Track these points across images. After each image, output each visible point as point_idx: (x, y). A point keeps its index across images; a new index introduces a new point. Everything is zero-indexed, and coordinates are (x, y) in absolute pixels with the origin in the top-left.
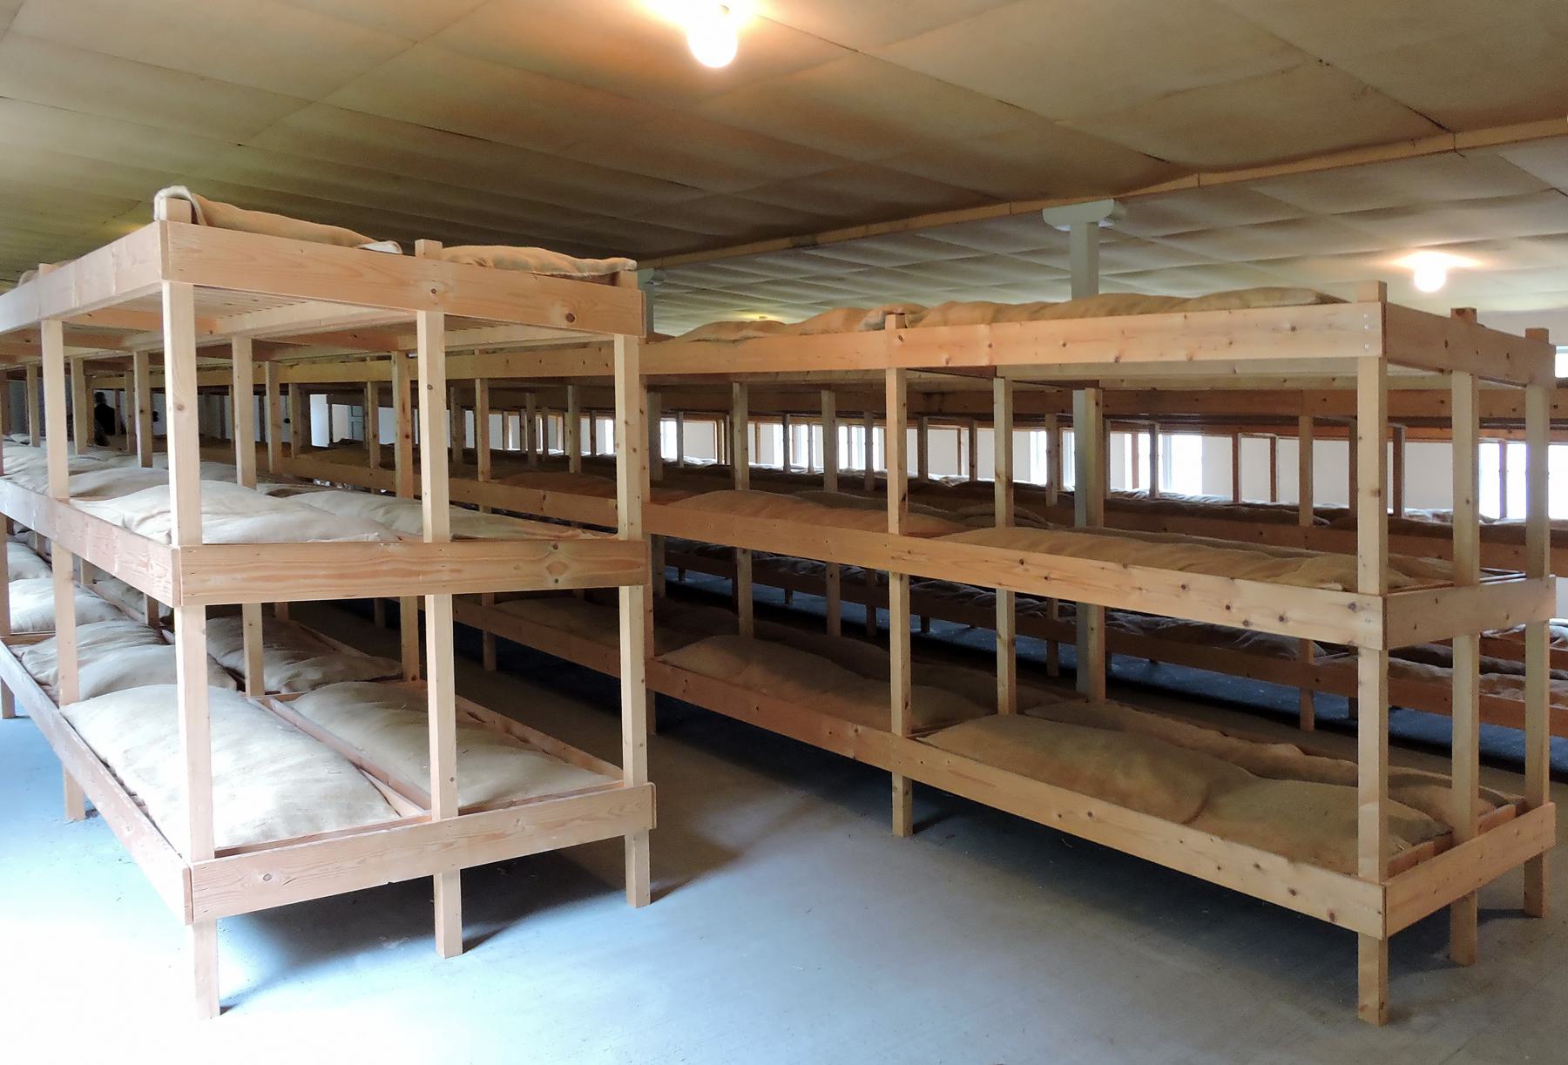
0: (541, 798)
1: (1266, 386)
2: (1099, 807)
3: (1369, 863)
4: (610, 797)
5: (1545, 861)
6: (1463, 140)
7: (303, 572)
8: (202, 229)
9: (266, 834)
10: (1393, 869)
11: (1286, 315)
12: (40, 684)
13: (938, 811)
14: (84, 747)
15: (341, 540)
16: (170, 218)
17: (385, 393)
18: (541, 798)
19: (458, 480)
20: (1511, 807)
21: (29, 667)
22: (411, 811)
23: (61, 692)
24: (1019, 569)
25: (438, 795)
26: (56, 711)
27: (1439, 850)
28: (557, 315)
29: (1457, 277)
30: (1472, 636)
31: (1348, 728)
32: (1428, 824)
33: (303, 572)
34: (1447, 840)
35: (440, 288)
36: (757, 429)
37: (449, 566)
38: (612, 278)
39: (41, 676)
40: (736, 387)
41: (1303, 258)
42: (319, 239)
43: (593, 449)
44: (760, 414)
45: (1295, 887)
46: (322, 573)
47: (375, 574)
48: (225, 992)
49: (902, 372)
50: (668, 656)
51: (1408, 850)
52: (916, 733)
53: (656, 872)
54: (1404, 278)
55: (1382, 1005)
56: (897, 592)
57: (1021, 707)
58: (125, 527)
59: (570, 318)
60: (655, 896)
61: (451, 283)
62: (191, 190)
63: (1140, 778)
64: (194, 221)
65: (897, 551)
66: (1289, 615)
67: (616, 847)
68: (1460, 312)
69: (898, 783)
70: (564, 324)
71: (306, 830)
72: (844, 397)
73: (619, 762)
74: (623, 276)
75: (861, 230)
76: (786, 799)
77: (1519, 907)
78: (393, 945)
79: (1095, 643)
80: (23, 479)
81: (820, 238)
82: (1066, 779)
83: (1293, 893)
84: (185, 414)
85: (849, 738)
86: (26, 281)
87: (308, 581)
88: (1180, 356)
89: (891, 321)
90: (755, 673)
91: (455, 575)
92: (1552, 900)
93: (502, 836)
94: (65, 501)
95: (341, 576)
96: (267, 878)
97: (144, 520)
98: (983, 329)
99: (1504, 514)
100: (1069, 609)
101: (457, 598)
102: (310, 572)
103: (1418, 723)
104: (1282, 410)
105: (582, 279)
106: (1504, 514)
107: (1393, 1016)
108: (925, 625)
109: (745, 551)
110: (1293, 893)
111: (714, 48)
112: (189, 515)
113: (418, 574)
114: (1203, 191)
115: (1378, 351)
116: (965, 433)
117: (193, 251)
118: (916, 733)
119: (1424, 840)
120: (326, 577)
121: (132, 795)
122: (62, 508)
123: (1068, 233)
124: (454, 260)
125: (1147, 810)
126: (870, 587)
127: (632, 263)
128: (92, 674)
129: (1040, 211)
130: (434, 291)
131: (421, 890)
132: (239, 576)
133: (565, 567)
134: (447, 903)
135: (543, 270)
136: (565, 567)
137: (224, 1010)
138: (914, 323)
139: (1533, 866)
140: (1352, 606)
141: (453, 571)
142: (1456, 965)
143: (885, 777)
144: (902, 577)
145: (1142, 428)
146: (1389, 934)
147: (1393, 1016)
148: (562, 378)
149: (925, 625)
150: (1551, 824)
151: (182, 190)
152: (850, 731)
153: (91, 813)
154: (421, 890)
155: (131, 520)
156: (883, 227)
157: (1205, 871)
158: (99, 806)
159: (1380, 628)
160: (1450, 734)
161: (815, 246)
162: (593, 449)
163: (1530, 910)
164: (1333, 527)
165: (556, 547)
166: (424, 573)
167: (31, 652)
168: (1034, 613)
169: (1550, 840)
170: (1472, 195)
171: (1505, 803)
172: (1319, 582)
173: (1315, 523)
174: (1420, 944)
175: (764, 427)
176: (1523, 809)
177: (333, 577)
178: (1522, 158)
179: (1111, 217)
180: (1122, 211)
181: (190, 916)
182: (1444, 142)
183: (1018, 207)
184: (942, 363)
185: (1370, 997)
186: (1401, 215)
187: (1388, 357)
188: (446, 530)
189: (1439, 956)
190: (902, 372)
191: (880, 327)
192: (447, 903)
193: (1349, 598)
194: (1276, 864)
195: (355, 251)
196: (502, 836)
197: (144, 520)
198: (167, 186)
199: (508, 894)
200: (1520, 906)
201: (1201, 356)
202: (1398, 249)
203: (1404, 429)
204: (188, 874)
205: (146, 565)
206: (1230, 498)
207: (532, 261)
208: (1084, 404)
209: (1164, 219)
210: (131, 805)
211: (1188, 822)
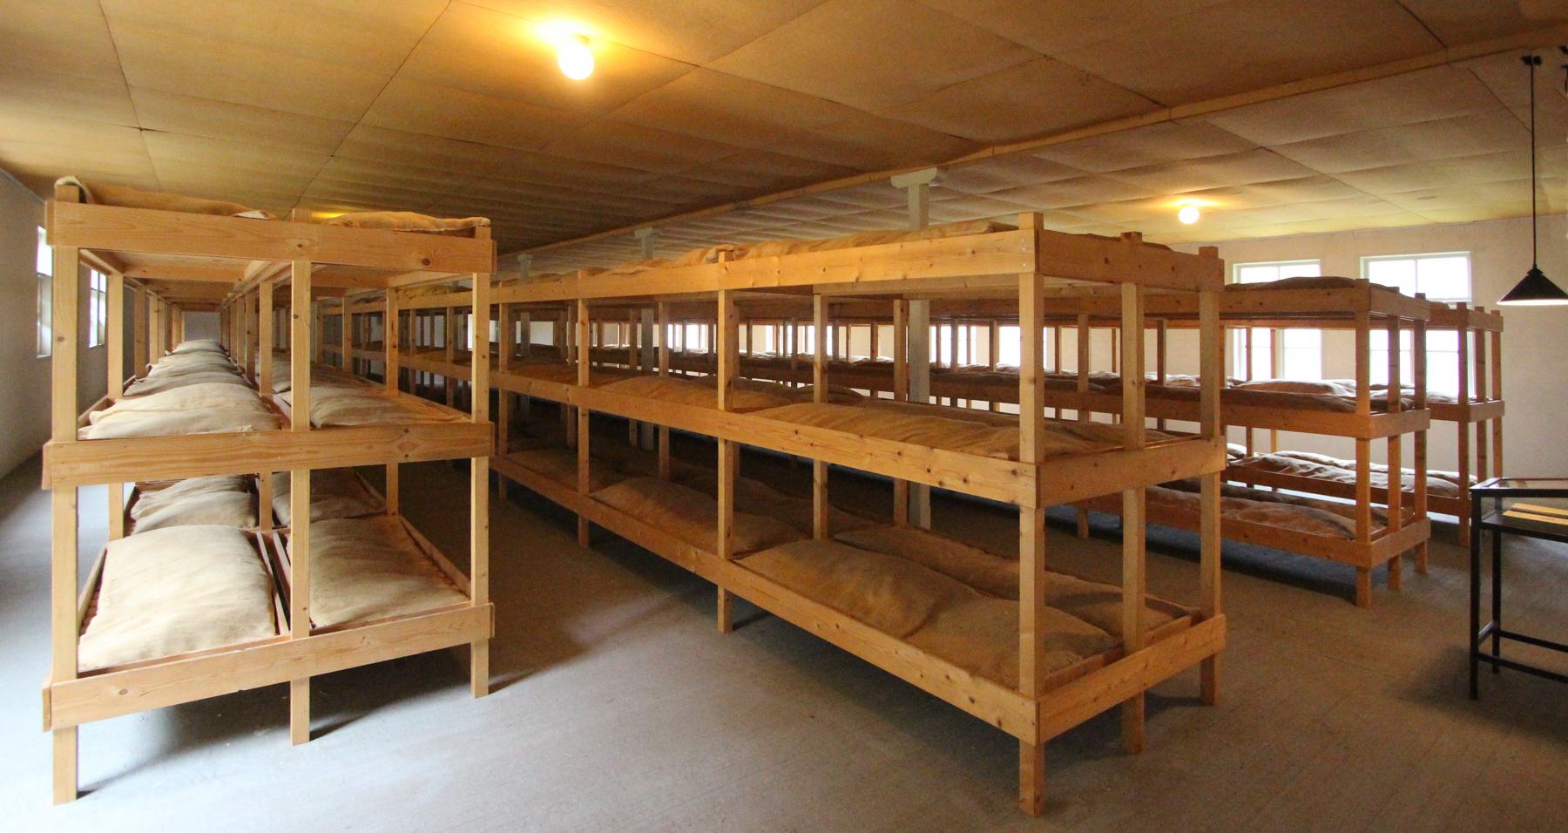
0: (394, 619)
1: (998, 296)
2: (844, 621)
3: (1027, 681)
4: (460, 615)
5: (1217, 662)
6: (1177, 112)
8: (91, 208)
9: (143, 655)
10: (1048, 686)
11: (969, 241)
18: (394, 619)
20: (1187, 619)
24: (795, 438)
25: (347, 620)
27: (1109, 661)
29: (1208, 215)
30: (1138, 490)
31: (1115, 537)
32: (1102, 639)
34: (1118, 652)
35: (306, 243)
36: (749, 329)
40: (817, 301)
41: (1094, 205)
43: (600, 342)
44: (675, 319)
45: (975, 697)
48: (82, 785)
49: (728, 293)
50: (598, 494)
51: (1079, 662)
52: (736, 556)
53: (493, 670)
54: (1171, 217)
55: (1037, 800)
57: (831, 531)
59: (426, 262)
60: (493, 689)
63: (882, 600)
66: (970, 478)
67: (465, 649)
68: (1127, 235)
69: (721, 593)
72: (711, 308)
74: (478, 231)
75: (775, 196)
76: (659, 597)
77: (1186, 700)
78: (260, 734)
81: (751, 203)
82: (826, 599)
83: (972, 701)
85: (692, 559)
88: (898, 276)
89: (722, 255)
90: (648, 507)
92: (1225, 689)
93: (349, 650)
95: (204, 460)
96: (123, 692)
98: (775, 259)
99: (1249, 377)
103: (1168, 533)
104: (1068, 311)
105: (440, 233)
106: (1249, 377)
107: (1048, 807)
110: (972, 701)
113: (276, 455)
114: (996, 159)
115: (1032, 268)
118: (736, 556)
119: (1097, 652)
125: (879, 626)
127: (486, 220)
131: (283, 689)
132: (106, 463)
133: (415, 446)
134: (300, 702)
135: (402, 228)
136: (415, 446)
137: (80, 794)
138: (740, 257)
139: (1208, 664)
140: (1014, 472)
142: (1126, 753)
143: (713, 588)
145: (961, 323)
146: (1044, 739)
147: (1048, 807)
148: (562, 302)
150: (1221, 630)
154: (283, 689)
156: (791, 193)
157: (912, 678)
159: (1033, 490)
160: (1147, 560)
161: (749, 208)
162: (600, 342)
163: (1205, 699)
164: (1104, 392)
169: (1220, 644)
170: (1211, 154)
171: (1185, 614)
172: (991, 452)
173: (1091, 389)
174: (1091, 741)
175: (756, 329)
176: (1198, 619)
178: (1222, 122)
179: (936, 180)
180: (943, 176)
181: (48, 724)
182: (1163, 115)
183: (876, 176)
184: (775, 284)
185: (1027, 794)
186: (1159, 171)
187: (1040, 271)
189: (1113, 744)
190: (728, 293)
191: (715, 260)
192: (300, 702)
193: (1013, 465)
194: (961, 676)
195: (228, 220)
196: (349, 650)
199: (348, 695)
200: (1197, 695)
201: (913, 275)
203: (1166, 322)
204: (48, 694)
209: (986, 181)
211: (905, 638)
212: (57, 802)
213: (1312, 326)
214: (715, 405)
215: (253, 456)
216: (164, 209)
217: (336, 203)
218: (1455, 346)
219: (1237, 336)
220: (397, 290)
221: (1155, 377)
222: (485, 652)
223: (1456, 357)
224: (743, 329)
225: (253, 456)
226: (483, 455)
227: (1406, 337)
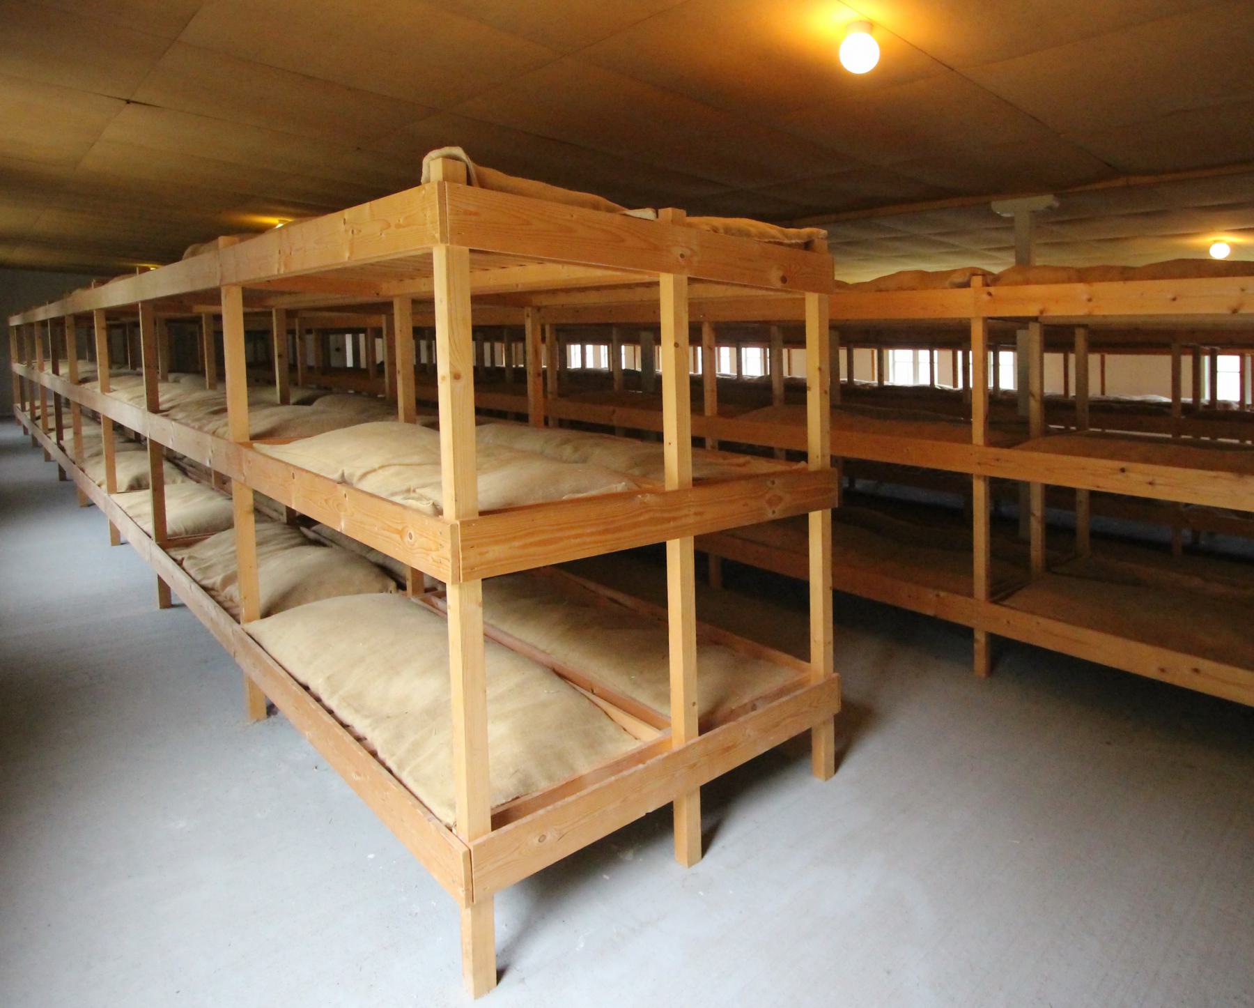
7: (573, 532)
8: (475, 190)
12: (205, 588)
13: (1005, 652)
14: (283, 674)
15: (593, 493)
16: (446, 178)
17: (378, 333)
19: (798, 448)
21: (192, 572)
22: (649, 735)
23: (243, 612)
24: (1120, 476)
25: (668, 712)
26: (236, 626)
28: (775, 275)
33: (573, 532)
35: (687, 252)
37: (693, 510)
38: (808, 245)
39: (205, 582)
40: (774, 329)
42: (582, 204)
46: (594, 529)
47: (635, 525)
56: (980, 490)
58: (343, 481)
59: (784, 280)
61: (695, 248)
62: (467, 152)
64: (469, 183)
65: (975, 457)
69: (980, 637)
70: (779, 285)
71: (563, 776)
73: (805, 655)
78: (629, 856)
79: (1037, 504)
80: (180, 416)
84: (460, 384)
85: (930, 601)
86: (193, 254)
87: (578, 541)
91: (699, 518)
94: (250, 447)
95: (606, 531)
96: (542, 838)
97: (365, 475)
100: (1072, 492)
101: (698, 540)
102: (579, 531)
105: (790, 245)
108: (852, 482)
109: (781, 450)
111: (859, 57)
112: (463, 484)
116: (876, 352)
117: (471, 214)
120: (592, 534)
121: (359, 739)
122: (244, 450)
123: (1011, 220)
124: (690, 225)
126: (962, 483)
128: (265, 590)
129: (988, 203)
130: (682, 256)
132: (517, 544)
136: (780, 499)
141: (696, 514)
143: (967, 633)
144: (985, 478)
149: (852, 482)
151: (458, 151)
152: (931, 595)
153: (271, 709)
155: (352, 475)
158: (278, 703)
165: (773, 483)
166: (674, 519)
167: (190, 558)
168: (1058, 496)
177: (599, 533)
188: (689, 474)
190: (986, 319)
191: (967, 285)
196: (734, 746)
197: (365, 475)
198: (439, 146)
202: (1210, 229)
205: (401, 533)
206: (1062, 392)
207: (753, 230)
208: (1080, 339)
210: (363, 754)
212: (478, 994)
213: (1163, 353)
214: (968, 439)
215: (652, 521)
216: (540, 198)
217: (283, 203)
218: (1238, 369)
219: (604, 364)
220: (539, 309)
221: (1189, 400)
222: (831, 729)
223: (1238, 376)
224: (843, 353)
225: (652, 521)
226: (826, 508)
227: (1187, 361)
